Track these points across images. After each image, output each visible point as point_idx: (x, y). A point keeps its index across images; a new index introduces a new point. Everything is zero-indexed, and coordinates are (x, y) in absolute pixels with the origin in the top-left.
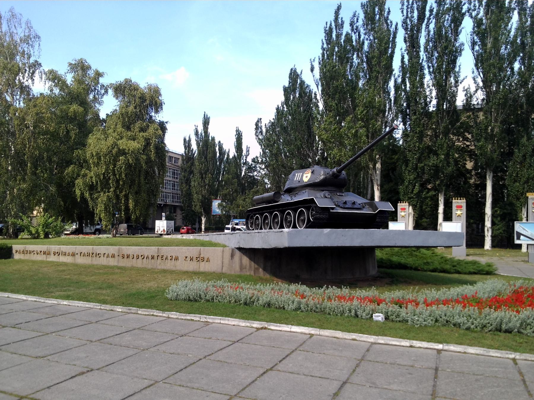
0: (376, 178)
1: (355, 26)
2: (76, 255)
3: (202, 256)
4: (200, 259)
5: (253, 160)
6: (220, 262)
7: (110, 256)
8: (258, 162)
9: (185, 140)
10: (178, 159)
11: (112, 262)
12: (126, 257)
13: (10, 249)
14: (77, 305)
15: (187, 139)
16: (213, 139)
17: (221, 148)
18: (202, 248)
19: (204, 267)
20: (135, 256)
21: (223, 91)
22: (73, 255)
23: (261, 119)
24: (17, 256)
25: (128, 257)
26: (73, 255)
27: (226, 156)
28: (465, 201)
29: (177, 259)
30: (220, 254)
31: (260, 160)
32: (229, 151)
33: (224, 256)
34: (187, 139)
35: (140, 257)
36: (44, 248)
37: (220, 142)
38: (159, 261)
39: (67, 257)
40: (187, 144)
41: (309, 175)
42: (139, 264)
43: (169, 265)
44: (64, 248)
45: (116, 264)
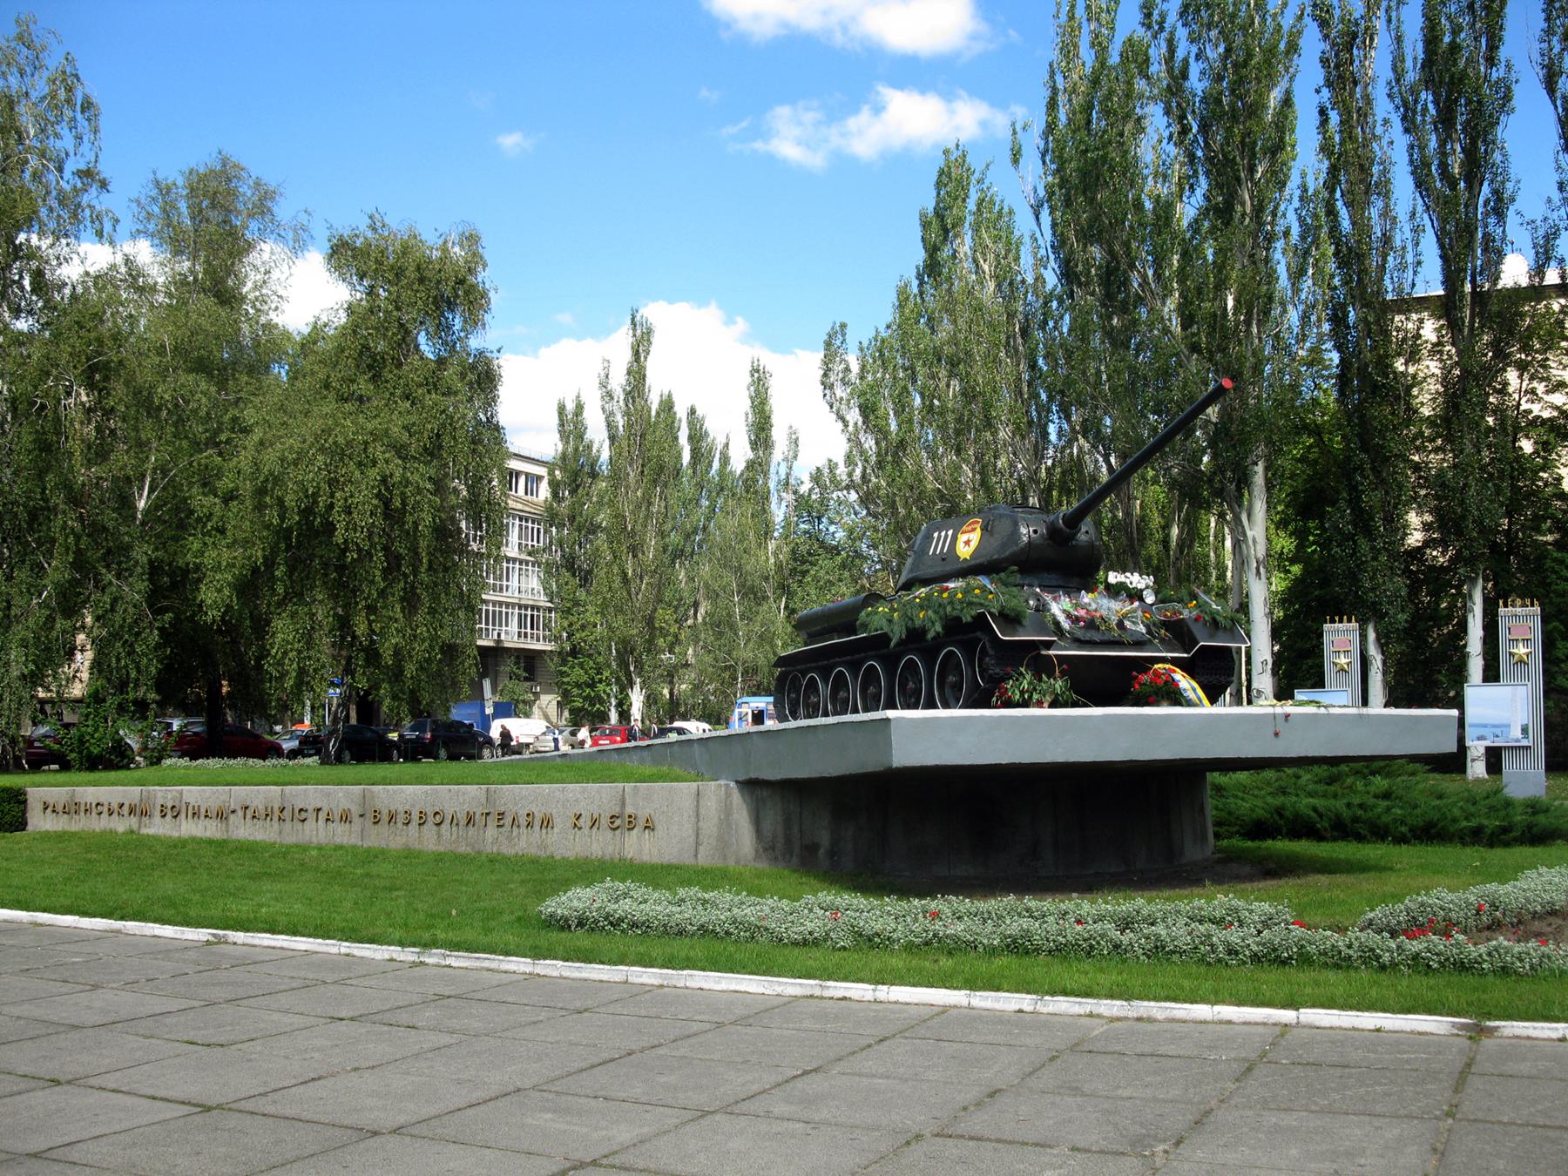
0: (1249, 534)
1: (1156, 12)
2: (232, 817)
3: (629, 810)
4: (622, 822)
5: (817, 478)
6: (688, 831)
7: (337, 818)
8: (837, 485)
9: (561, 409)
10: (540, 478)
11: (342, 835)
12: (385, 818)
13: (18, 798)
14: (266, 943)
15: (570, 407)
16: (667, 405)
17: (697, 437)
18: (629, 786)
19: (637, 846)
20: (415, 816)
21: (706, 330)
22: (222, 815)
23: (843, 326)
24: (39, 822)
25: (392, 818)
26: (222, 815)
27: (716, 465)
28: (1537, 609)
29: (547, 823)
30: (688, 804)
31: (842, 471)
32: (727, 445)
33: (702, 811)
34: (570, 407)
35: (430, 819)
36: (132, 793)
37: (693, 411)
38: (491, 831)
39: (203, 822)
40: (571, 424)
41: (975, 537)
42: (428, 840)
43: (523, 844)
44: (193, 794)
45: (354, 840)
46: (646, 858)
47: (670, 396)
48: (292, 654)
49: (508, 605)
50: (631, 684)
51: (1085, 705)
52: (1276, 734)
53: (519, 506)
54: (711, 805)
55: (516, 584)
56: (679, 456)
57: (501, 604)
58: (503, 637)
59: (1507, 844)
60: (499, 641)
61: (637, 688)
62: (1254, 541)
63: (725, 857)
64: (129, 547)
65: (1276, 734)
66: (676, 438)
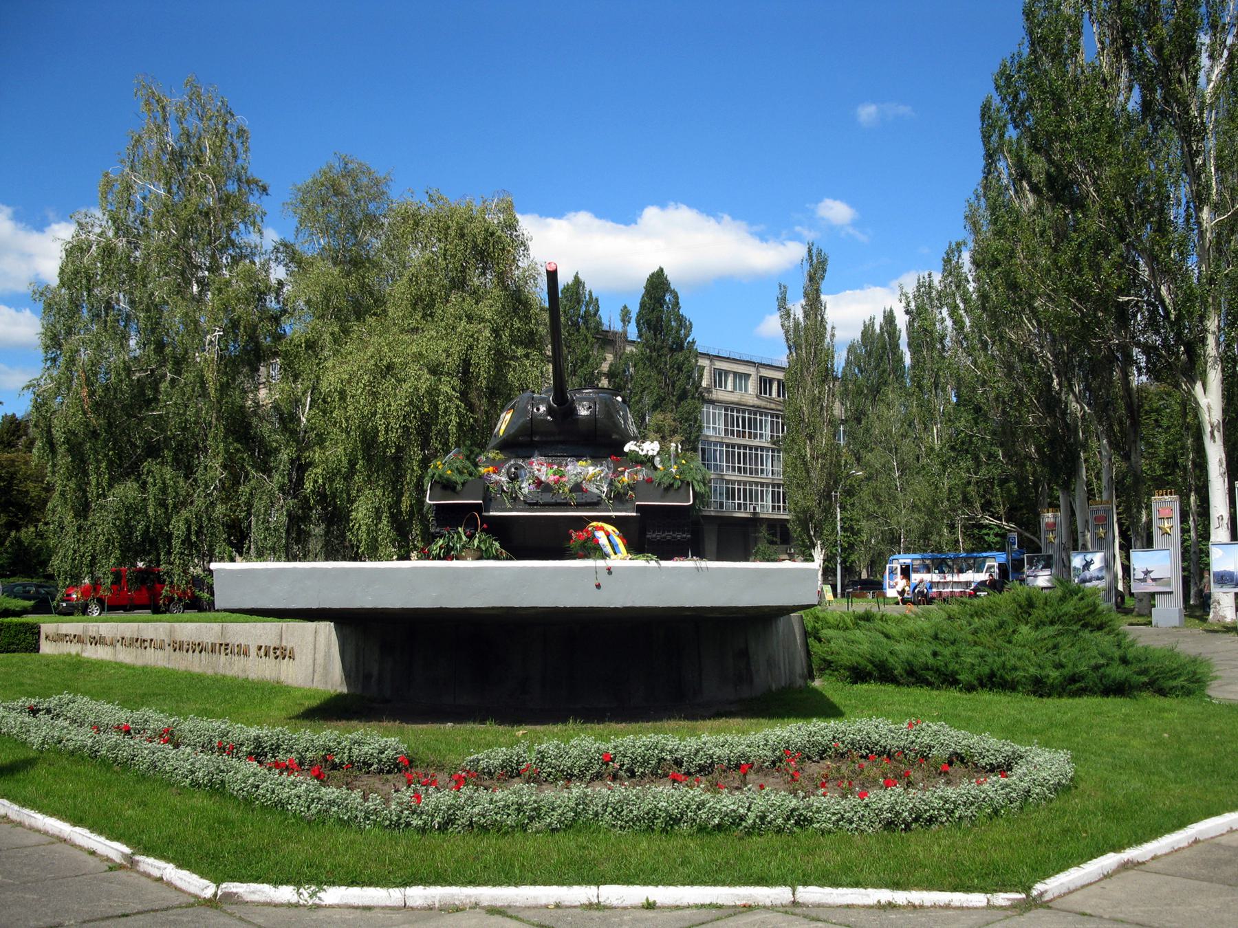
3: (284, 644)
13: (35, 631)
18: (176, 625)
24: (46, 648)
46: (290, 681)
47: (891, 311)
48: (364, 528)
49: (762, 484)
50: (813, 546)
51: (511, 559)
52: (598, 586)
53: (773, 406)
54: (322, 639)
55: (770, 468)
56: (901, 360)
57: (757, 484)
58: (758, 510)
59: (1074, 694)
60: (755, 513)
61: (818, 549)
62: (1209, 408)
63: (326, 683)
64: (277, 450)
65: (598, 586)
66: (898, 345)
